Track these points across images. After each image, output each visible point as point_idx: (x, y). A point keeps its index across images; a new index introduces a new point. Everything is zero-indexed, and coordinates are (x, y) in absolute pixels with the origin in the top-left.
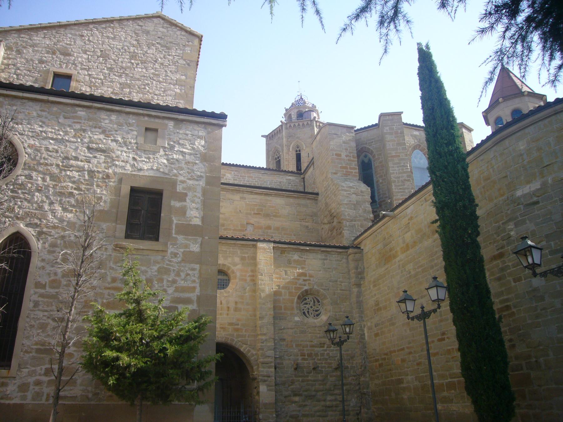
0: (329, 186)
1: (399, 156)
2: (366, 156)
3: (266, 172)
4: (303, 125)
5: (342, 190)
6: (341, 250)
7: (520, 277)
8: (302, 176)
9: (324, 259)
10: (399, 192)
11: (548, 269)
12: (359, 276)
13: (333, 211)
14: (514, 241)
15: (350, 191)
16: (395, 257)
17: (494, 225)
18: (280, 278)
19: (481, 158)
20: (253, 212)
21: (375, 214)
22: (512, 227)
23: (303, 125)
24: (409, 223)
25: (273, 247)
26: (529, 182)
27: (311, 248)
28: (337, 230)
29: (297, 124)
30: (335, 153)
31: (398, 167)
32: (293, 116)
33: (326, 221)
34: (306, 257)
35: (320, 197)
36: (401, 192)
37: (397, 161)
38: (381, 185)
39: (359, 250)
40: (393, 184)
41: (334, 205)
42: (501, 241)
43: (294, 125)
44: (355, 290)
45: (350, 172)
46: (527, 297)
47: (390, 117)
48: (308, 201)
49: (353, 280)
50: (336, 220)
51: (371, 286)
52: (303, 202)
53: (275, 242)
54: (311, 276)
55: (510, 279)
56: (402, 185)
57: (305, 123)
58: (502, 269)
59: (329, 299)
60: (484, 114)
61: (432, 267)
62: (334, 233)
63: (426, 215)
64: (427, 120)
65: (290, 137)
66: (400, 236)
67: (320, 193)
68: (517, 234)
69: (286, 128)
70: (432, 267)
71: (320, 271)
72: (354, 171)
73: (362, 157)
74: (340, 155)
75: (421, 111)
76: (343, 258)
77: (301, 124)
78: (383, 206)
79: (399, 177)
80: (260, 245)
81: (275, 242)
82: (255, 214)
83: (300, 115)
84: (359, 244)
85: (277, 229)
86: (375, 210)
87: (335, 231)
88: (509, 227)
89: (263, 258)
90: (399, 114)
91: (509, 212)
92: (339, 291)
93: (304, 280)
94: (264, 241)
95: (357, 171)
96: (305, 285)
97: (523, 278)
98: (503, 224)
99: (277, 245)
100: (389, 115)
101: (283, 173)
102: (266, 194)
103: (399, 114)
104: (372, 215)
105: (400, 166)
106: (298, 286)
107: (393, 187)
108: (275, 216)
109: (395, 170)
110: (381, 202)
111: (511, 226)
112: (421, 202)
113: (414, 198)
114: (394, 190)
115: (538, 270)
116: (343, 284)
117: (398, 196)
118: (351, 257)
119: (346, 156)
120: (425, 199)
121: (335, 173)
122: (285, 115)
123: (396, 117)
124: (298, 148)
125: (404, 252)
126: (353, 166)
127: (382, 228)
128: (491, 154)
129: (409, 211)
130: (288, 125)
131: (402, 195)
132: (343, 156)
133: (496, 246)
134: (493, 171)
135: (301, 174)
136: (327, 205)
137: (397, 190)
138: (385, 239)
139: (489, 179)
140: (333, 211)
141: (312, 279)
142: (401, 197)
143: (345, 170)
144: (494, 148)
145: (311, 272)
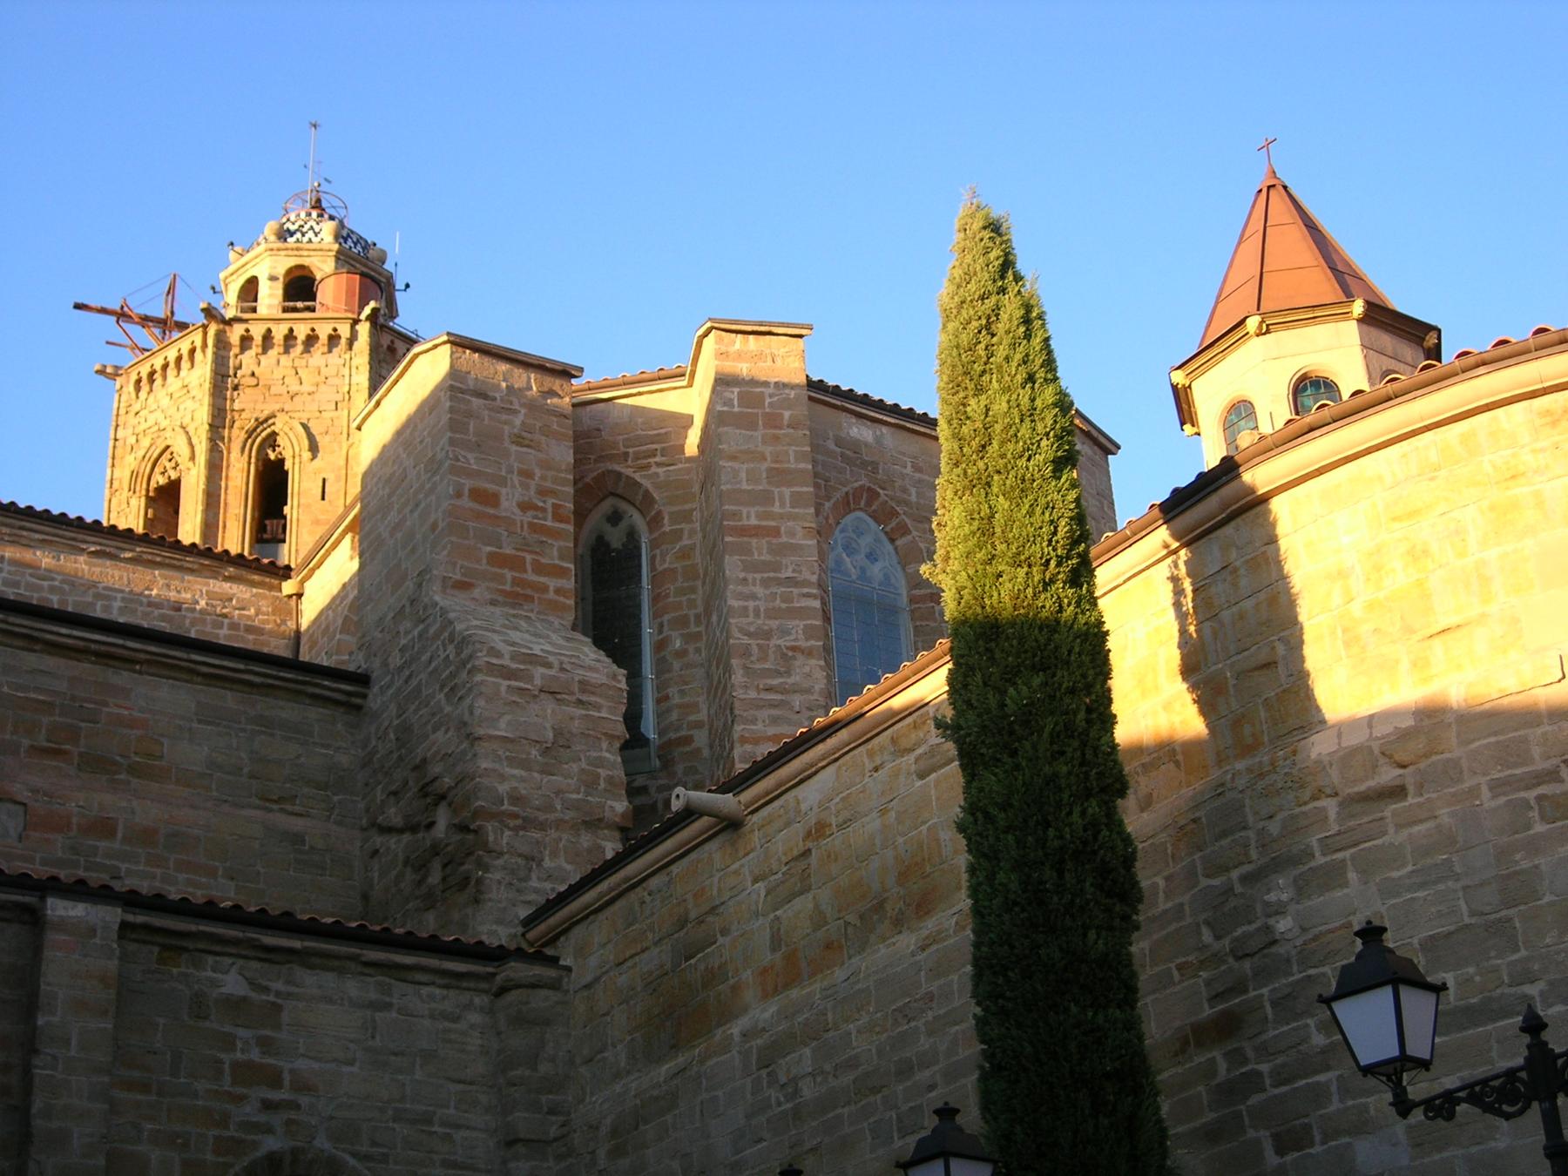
1: (776, 532)
2: (615, 518)
5: (492, 669)
6: (461, 967)
9: (374, 1006)
10: (759, 705)
11: (1458, 1084)
13: (436, 769)
15: (530, 679)
16: (727, 1014)
17: (1204, 882)
20: (26, 742)
21: (639, 800)
25: (124, 926)
28: (456, 866)
30: (468, 484)
31: (766, 583)
34: (279, 986)
35: (376, 699)
36: (773, 705)
37: (766, 557)
38: (676, 665)
39: (551, 973)
40: (735, 662)
41: (442, 739)
45: (532, 585)
48: (314, 713)
50: (443, 818)
51: (602, 1153)
54: (302, 1086)
56: (779, 674)
58: (1232, 1092)
62: (435, 878)
68: (1304, 930)
71: (351, 1063)
72: (552, 583)
73: (596, 518)
74: (491, 499)
76: (469, 1006)
78: (679, 769)
79: (767, 635)
80: (59, 908)
81: (132, 900)
82: (36, 750)
85: (146, 836)
86: (640, 781)
87: (436, 865)
88: (1272, 897)
93: (268, 1106)
94: (79, 890)
95: (569, 584)
96: (268, 1130)
98: (1245, 879)
102: (105, 657)
105: (780, 582)
106: (231, 1132)
107: (738, 678)
108: (133, 770)
109: (754, 597)
110: (669, 743)
114: (739, 693)
115: (1419, 1087)
116: (459, 1135)
117: (754, 721)
119: (525, 507)
120: (894, 741)
121: (463, 586)
125: (776, 991)
126: (552, 557)
129: (809, 794)
131: (775, 721)
132: (509, 504)
133: (1208, 983)
136: (405, 730)
137: (753, 694)
138: (682, 922)
140: (436, 769)
141: (304, 1100)
142: (771, 731)
143: (509, 575)
145: (301, 1064)
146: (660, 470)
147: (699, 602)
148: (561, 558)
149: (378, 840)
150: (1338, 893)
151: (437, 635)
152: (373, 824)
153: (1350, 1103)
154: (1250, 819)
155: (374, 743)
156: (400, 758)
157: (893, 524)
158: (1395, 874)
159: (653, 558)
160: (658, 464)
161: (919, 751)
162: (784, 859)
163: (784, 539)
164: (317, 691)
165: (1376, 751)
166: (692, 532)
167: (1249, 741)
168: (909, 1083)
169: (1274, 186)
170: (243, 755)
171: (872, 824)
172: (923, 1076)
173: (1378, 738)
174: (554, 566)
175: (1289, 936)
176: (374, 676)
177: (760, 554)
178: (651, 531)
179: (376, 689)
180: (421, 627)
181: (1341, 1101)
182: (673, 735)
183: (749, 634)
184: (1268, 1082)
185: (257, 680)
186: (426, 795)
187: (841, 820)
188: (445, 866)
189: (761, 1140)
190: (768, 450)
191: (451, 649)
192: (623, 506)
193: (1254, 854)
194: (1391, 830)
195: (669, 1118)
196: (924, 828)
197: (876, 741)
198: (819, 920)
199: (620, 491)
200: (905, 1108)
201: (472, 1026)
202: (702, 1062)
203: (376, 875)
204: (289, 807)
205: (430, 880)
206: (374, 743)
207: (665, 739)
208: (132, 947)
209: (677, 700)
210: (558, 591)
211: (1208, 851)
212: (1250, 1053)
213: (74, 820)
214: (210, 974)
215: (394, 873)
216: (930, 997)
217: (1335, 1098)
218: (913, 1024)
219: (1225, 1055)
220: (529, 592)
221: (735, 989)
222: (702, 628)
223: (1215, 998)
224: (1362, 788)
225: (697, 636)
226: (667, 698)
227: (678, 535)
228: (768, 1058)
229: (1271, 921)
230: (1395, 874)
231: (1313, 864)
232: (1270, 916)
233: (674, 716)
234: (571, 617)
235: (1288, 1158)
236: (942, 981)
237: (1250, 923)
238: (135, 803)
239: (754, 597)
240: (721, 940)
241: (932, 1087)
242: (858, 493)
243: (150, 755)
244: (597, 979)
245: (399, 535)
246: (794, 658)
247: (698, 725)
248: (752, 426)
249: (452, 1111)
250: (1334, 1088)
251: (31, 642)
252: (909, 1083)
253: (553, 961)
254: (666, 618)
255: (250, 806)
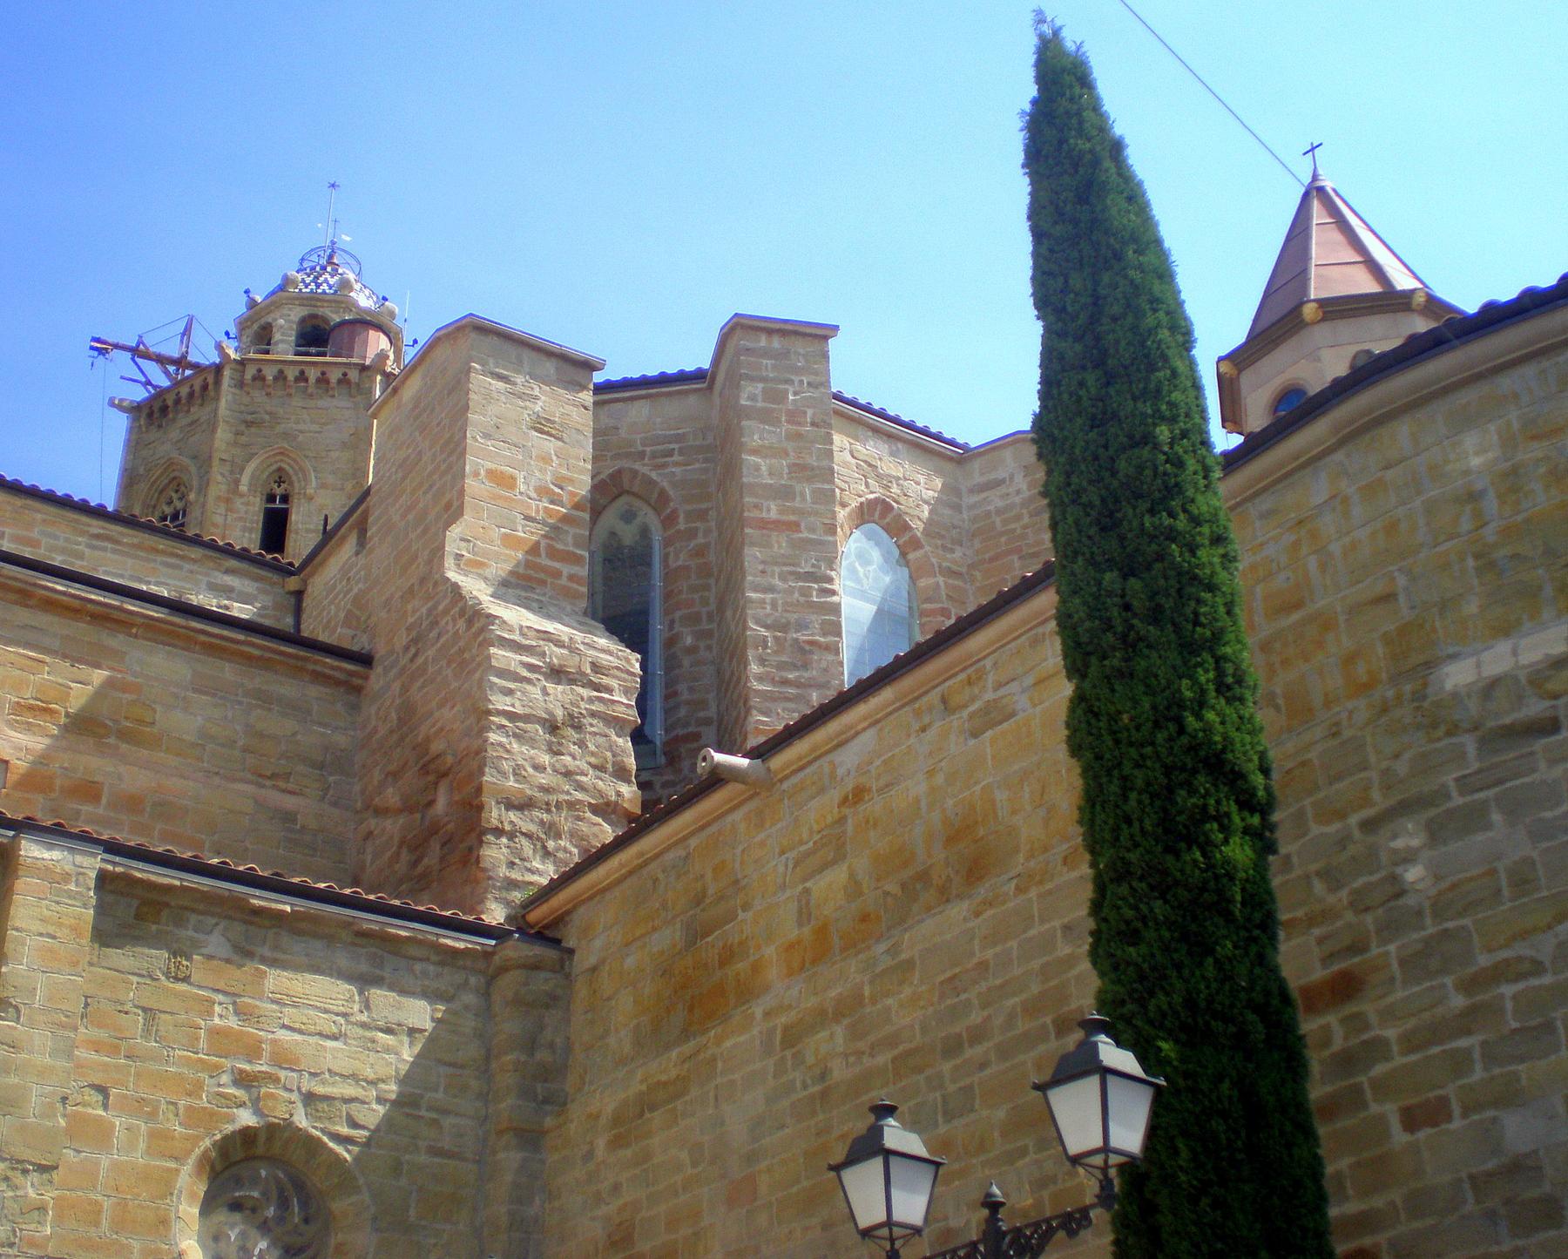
0: (435, 623)
3: (115, 529)
4: (323, 380)
7: (1443, 1102)
8: (293, 583)
12: (539, 1088)
13: (437, 746)
14: (1419, 913)
16: (747, 992)
18: (114, 1050)
19: (1266, 502)
22: (1415, 842)
23: (323, 380)
24: (842, 820)
25: (103, 879)
26: (1505, 630)
27: (303, 905)
29: (291, 373)
32: (277, 337)
33: (392, 796)
35: (377, 679)
38: (686, 662)
42: (1349, 916)
43: (280, 377)
44: (510, 1158)
45: (544, 569)
46: (1470, 1206)
47: (776, 343)
48: (314, 691)
49: (507, 1104)
51: (601, 1143)
52: (287, 688)
53: (113, 848)
54: (284, 1059)
55: (1390, 1110)
56: (795, 667)
57: (334, 376)
59: (366, 1197)
60: (1224, 368)
61: (952, 1048)
62: (431, 860)
63: (940, 779)
64: (1050, 274)
65: (249, 424)
66: (783, 887)
67: (380, 650)
68: (1438, 878)
69: (241, 384)
70: (952, 1048)
72: (566, 570)
73: (610, 519)
75: (1119, 129)
77: (313, 374)
79: (784, 628)
83: (315, 336)
84: (560, 920)
87: (435, 847)
88: (1399, 843)
89: (36, 926)
90: (819, 335)
91: (1402, 768)
92: (423, 1158)
93: (242, 1080)
94: (57, 832)
95: (583, 571)
97: (1457, 1111)
99: (119, 865)
100: (770, 332)
101: (196, 552)
103: (819, 335)
104: (628, 792)
108: (123, 735)
110: (677, 739)
111: (1409, 835)
112: (918, 714)
113: (887, 694)
116: (448, 1121)
118: (508, 984)
120: (944, 701)
122: (243, 324)
123: (799, 346)
124: (280, 482)
127: (693, 842)
128: (1318, 488)
129: (848, 758)
130: (250, 372)
133: (1320, 941)
134: (1323, 567)
135: (287, 571)
136: (408, 715)
138: (699, 900)
139: (1298, 605)
144: (1339, 456)
146: (677, 470)
147: (712, 600)
148: (577, 545)
149: (373, 823)
150: (1480, 837)
151: (446, 612)
152: (367, 807)
153: (1497, 1071)
154: (1373, 759)
155: (374, 723)
156: (402, 739)
157: (906, 538)
158: (1548, 814)
159: (666, 557)
160: (677, 464)
161: (971, 709)
162: (816, 827)
163: (805, 535)
164: (318, 668)
165: (1523, 680)
166: (707, 532)
167: (1364, 679)
168: (958, 1061)
169: (1315, 192)
170: (238, 727)
171: (916, 787)
172: (973, 1052)
173: (1524, 667)
174: (568, 552)
175: (1420, 886)
176: (377, 657)
177: (780, 547)
178: (665, 528)
179: (378, 669)
180: (430, 604)
181: (1486, 1069)
182: (680, 732)
183: (767, 627)
184: (1395, 1048)
185: (256, 652)
186: (428, 773)
187: (882, 782)
188: (443, 845)
189: (783, 1127)
190: (790, 446)
191: (461, 624)
192: (637, 503)
193: (1376, 795)
194: (1542, 765)
195: (679, 1104)
196: (978, 788)
197: (925, 699)
198: (854, 889)
199: (635, 489)
200: (952, 1088)
201: (467, 1008)
202: (718, 1044)
203: (369, 858)
204: (281, 784)
205: (426, 861)
206: (374, 723)
207: (673, 734)
208: (110, 898)
209: (685, 696)
210: (571, 578)
211: (1321, 795)
212: (1373, 1018)
213: (58, 782)
214: (190, 933)
215: (389, 854)
216: (983, 966)
217: (1478, 1067)
218: (963, 997)
219: (1343, 1021)
220: (542, 576)
221: (756, 968)
222: (714, 625)
223: (1327, 960)
224: (1507, 720)
225: (708, 634)
226: (675, 694)
227: (692, 533)
228: (792, 1037)
229: (1399, 870)
230: (1548, 814)
231: (1450, 805)
232: (1396, 864)
233: (682, 712)
234: (583, 604)
235: (1422, 1135)
236: (998, 949)
237: (1371, 873)
238: (122, 769)
239: (771, 589)
240: (741, 915)
241: (983, 1066)
242: (872, 504)
243: (140, 721)
244: (602, 962)
245: (410, 517)
246: (811, 652)
247: (707, 722)
248: (776, 422)
249: (440, 1095)
250: (1477, 1055)
251: (24, 596)
252: (958, 1061)
253: (556, 942)
254: (678, 614)
255: (242, 780)
